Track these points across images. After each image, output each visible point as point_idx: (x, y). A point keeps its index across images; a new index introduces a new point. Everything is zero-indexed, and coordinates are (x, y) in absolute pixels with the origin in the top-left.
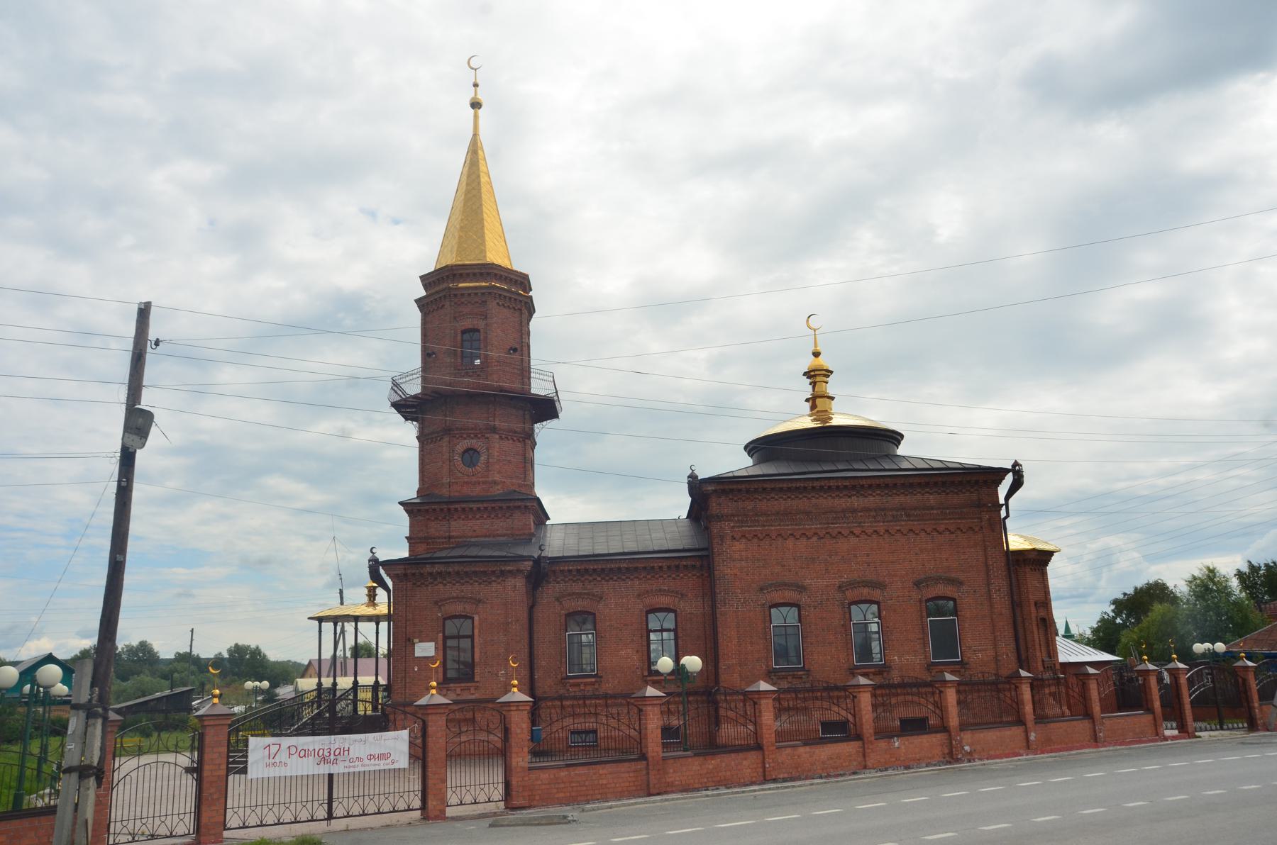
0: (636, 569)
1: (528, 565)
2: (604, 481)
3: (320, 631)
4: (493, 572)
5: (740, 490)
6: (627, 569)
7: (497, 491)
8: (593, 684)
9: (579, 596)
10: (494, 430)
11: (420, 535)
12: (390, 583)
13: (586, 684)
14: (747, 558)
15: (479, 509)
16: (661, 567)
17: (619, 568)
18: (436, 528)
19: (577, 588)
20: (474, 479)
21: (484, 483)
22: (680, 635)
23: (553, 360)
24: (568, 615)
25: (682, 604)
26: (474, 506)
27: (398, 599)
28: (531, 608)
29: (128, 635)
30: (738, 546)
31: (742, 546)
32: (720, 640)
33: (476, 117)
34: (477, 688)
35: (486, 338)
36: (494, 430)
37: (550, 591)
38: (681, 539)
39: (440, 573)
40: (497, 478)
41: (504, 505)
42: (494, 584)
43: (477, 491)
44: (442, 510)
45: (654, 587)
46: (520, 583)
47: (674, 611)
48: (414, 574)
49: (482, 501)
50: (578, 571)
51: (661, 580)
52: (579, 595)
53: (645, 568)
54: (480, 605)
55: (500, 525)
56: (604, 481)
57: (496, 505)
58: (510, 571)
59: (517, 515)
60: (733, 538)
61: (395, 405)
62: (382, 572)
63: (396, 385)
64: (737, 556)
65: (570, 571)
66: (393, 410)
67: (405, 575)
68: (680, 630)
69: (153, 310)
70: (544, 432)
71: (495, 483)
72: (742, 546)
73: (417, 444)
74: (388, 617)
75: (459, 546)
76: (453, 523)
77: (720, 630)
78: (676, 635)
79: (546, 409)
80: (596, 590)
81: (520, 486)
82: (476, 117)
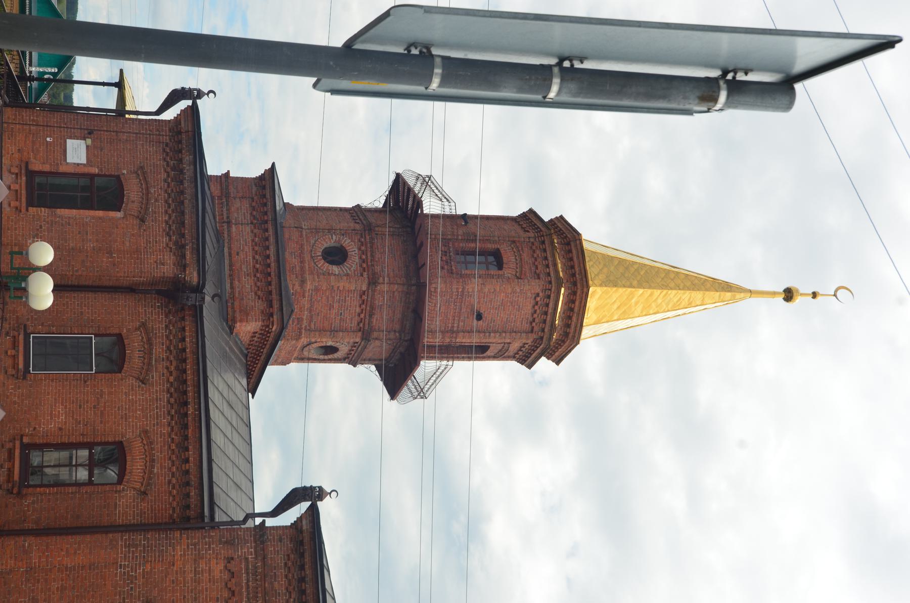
0: (185, 427)
1: (192, 276)
2: (308, 426)
3: (104, 84)
4: (183, 235)
5: (302, 567)
6: (186, 415)
7: (292, 284)
8: (15, 366)
9: (148, 352)
10: (373, 282)
11: (232, 190)
12: (170, 114)
13: (15, 357)
14: (198, 582)
15: (268, 257)
16: (187, 461)
17: (186, 404)
18: (241, 210)
19: (159, 350)
20: (307, 257)
21: (302, 268)
22: (84, 489)
23: (471, 389)
24: (119, 336)
25: (130, 493)
26: (272, 252)
27: (149, 128)
28: (131, 290)
29: (76, 86)
30: (218, 568)
31: (217, 574)
32: (71, 539)
33: (774, 294)
34: (18, 209)
35: (492, 277)
36: (373, 282)
37: (157, 319)
38: (229, 509)
39: (181, 171)
40: (309, 286)
41: (273, 288)
42: (165, 239)
43: (291, 260)
44: (266, 213)
45: (157, 454)
46: (168, 269)
47: (120, 482)
48: (180, 142)
49: (277, 242)
50: (184, 350)
51: (167, 463)
52: (148, 352)
53: (186, 438)
54: (136, 222)
55: (246, 285)
56: (308, 426)
57: (274, 279)
58: (183, 256)
59: (260, 305)
60: (230, 560)
61: (398, 176)
62: (184, 104)
63: (426, 181)
64: (202, 565)
65: (183, 340)
66: (393, 177)
67: (180, 133)
68: (89, 489)
69: (387, 396)
70: (368, 374)
71: (303, 282)
72: (217, 574)
73: (350, 205)
74: (121, 109)
75: (218, 235)
76: (248, 229)
77: (88, 538)
78: (83, 484)
79: (396, 378)
80: (155, 376)
81: (300, 320)
82: (774, 294)
